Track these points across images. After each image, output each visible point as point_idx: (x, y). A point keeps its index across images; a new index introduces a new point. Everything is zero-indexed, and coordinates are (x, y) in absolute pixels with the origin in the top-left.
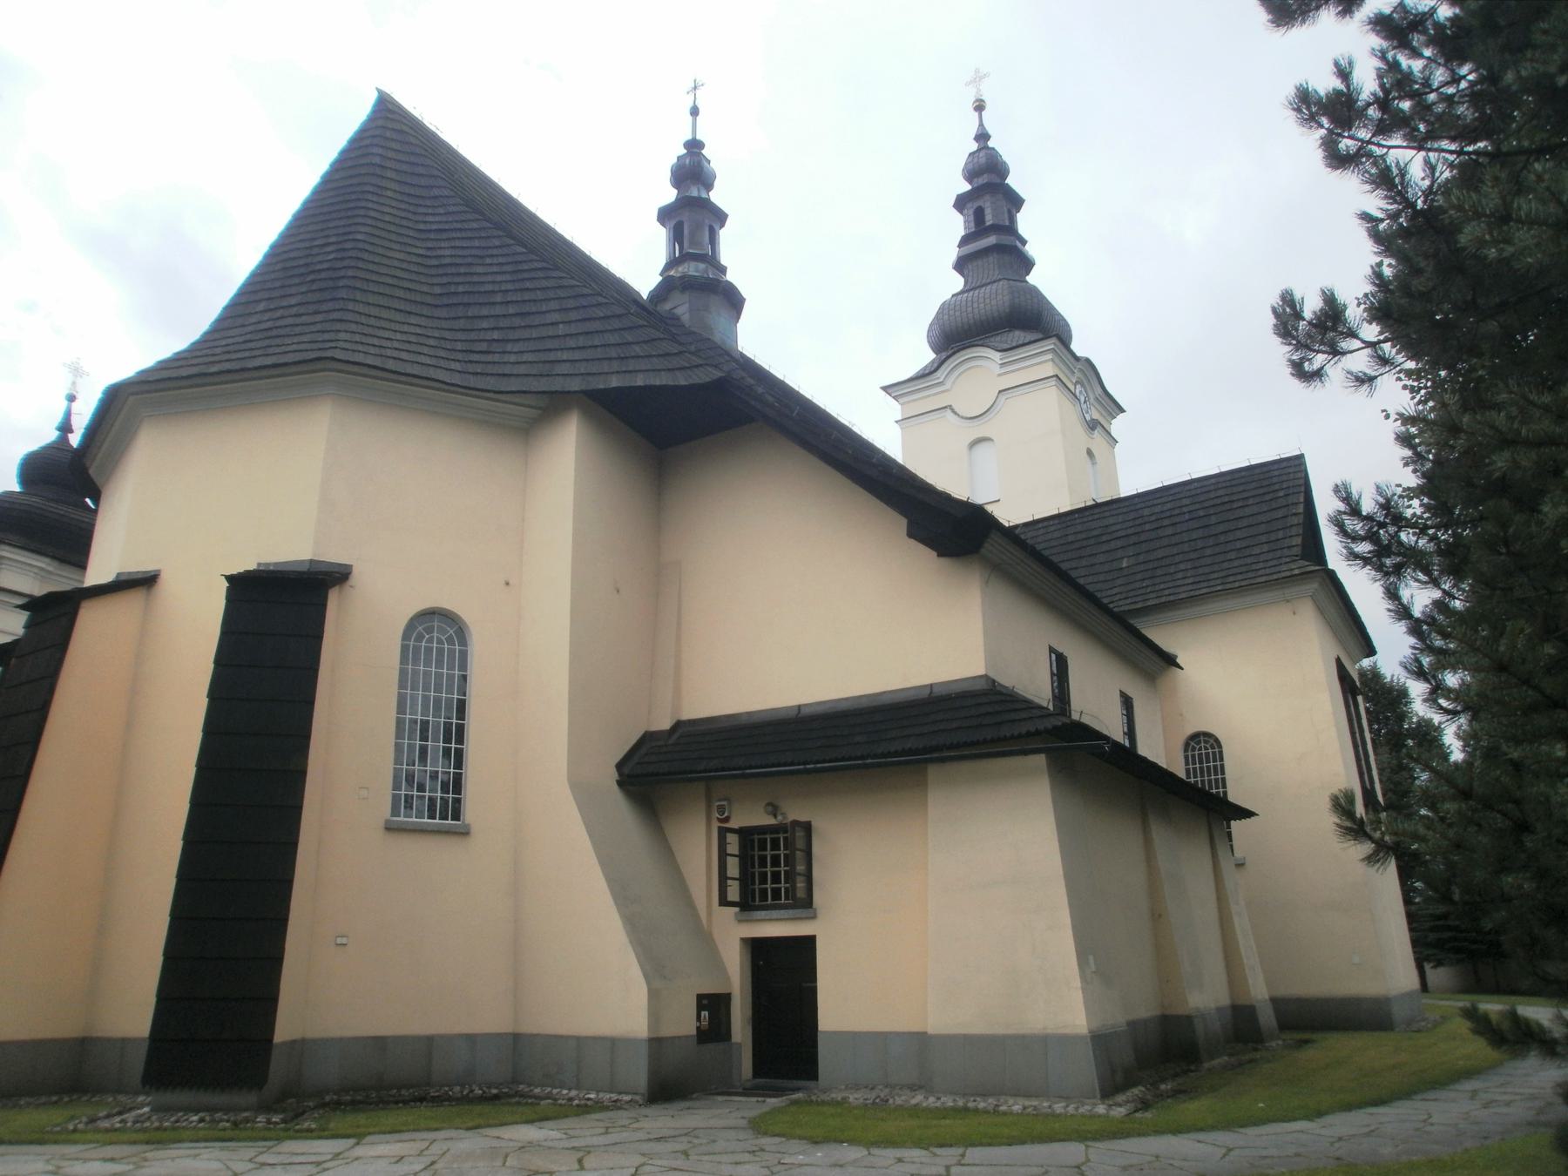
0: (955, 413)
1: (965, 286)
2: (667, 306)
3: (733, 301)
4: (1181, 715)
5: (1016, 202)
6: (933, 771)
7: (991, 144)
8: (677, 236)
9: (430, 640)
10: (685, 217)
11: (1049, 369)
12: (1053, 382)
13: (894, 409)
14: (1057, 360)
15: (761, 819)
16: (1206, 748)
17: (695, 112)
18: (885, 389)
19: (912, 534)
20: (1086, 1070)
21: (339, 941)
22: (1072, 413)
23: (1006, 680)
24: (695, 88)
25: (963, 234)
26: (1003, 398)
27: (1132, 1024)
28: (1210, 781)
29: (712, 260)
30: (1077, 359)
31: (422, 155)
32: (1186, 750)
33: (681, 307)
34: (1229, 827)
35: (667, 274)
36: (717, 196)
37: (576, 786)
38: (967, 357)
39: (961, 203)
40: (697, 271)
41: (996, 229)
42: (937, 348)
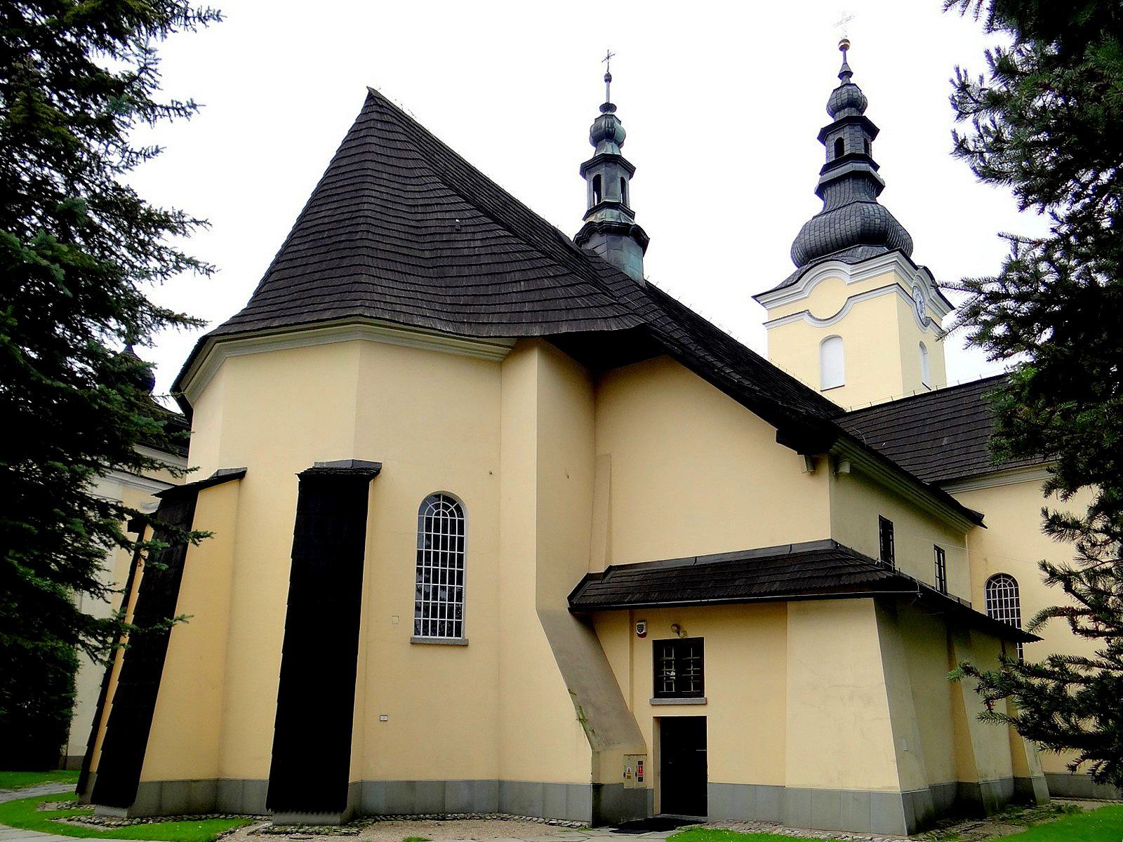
0: (811, 316)
1: (824, 208)
2: (590, 246)
3: (641, 239)
4: (986, 560)
5: (871, 131)
6: (791, 606)
7: (852, 80)
8: (596, 186)
9: (438, 514)
10: (602, 171)
11: (891, 278)
12: (895, 288)
13: (760, 313)
14: (898, 270)
15: (670, 635)
16: (1005, 586)
17: (608, 79)
18: (755, 297)
19: (781, 439)
20: (898, 818)
21: (382, 718)
22: (910, 312)
23: (844, 542)
24: (608, 58)
25: (825, 163)
26: (849, 300)
27: (934, 789)
28: (995, 612)
29: (622, 207)
30: (916, 268)
31: (390, 122)
32: (988, 587)
33: (599, 245)
34: (1021, 646)
35: (589, 220)
36: (627, 153)
37: (546, 618)
38: (827, 269)
39: (824, 135)
40: (612, 218)
41: (854, 157)
42: (799, 264)
